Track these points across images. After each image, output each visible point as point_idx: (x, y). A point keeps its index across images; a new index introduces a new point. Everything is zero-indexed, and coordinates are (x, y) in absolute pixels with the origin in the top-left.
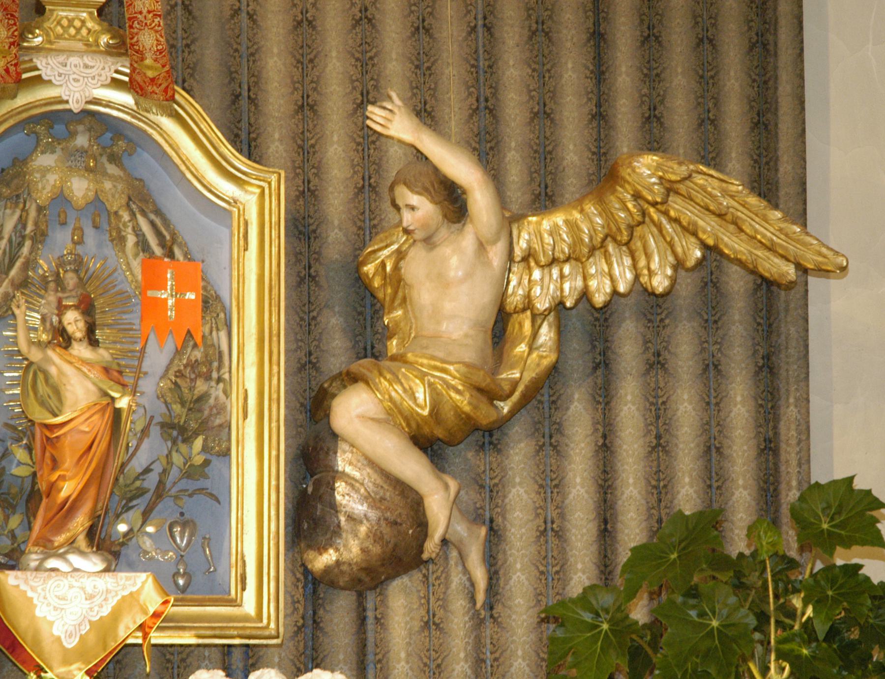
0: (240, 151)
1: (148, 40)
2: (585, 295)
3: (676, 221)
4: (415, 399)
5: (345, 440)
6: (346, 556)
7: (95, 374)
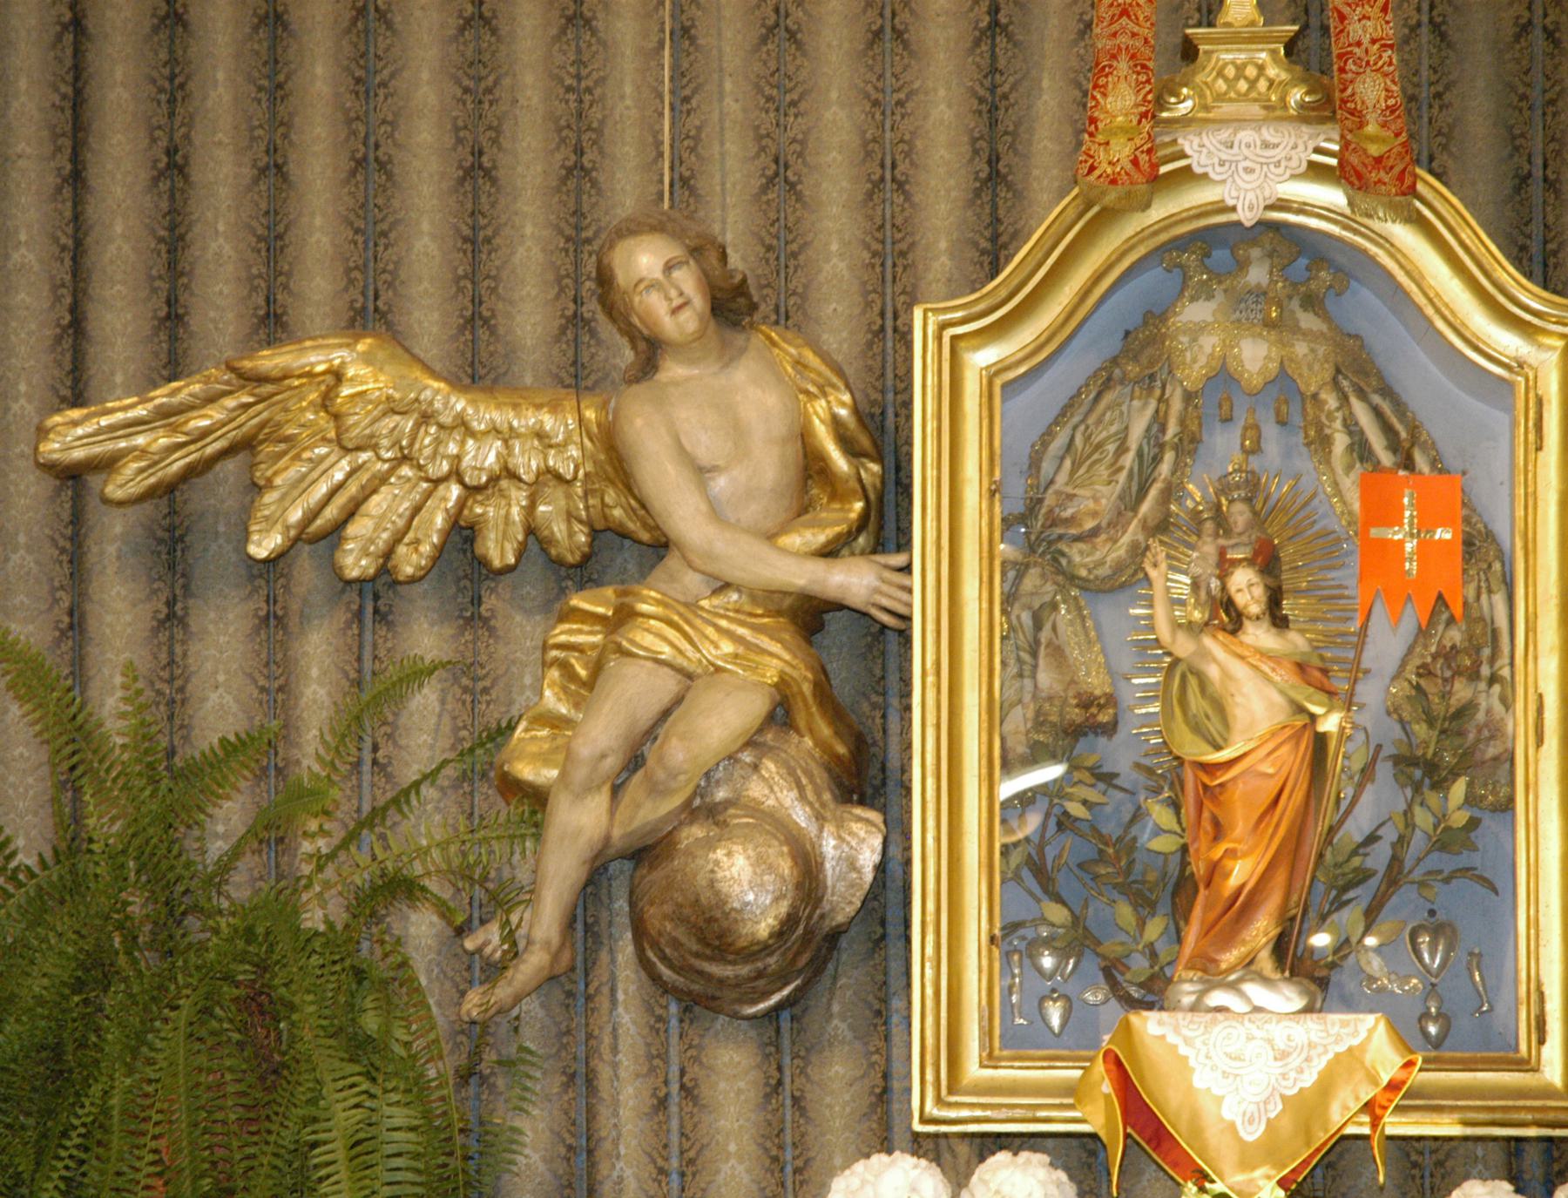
1: (1371, 91)
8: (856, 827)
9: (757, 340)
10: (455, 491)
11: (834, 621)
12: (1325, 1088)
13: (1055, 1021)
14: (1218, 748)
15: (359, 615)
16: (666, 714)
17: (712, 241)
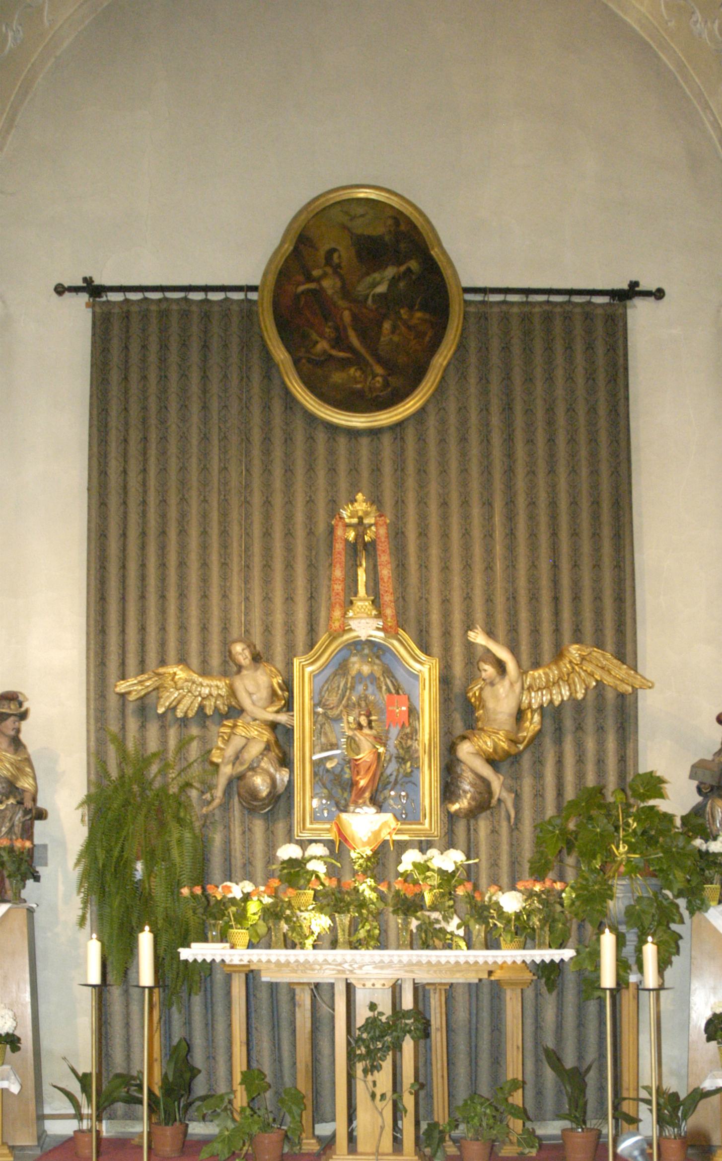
0: (422, 652)
1: (389, 612)
2: (551, 702)
3: (585, 671)
4: (487, 745)
5: (464, 763)
6: (463, 806)
7: (371, 739)
8: (284, 772)
9: (262, 665)
10: (200, 699)
11: (279, 727)
12: (380, 831)
13: (326, 815)
14: (357, 755)
15: (180, 726)
16: (243, 748)
17: (252, 644)
